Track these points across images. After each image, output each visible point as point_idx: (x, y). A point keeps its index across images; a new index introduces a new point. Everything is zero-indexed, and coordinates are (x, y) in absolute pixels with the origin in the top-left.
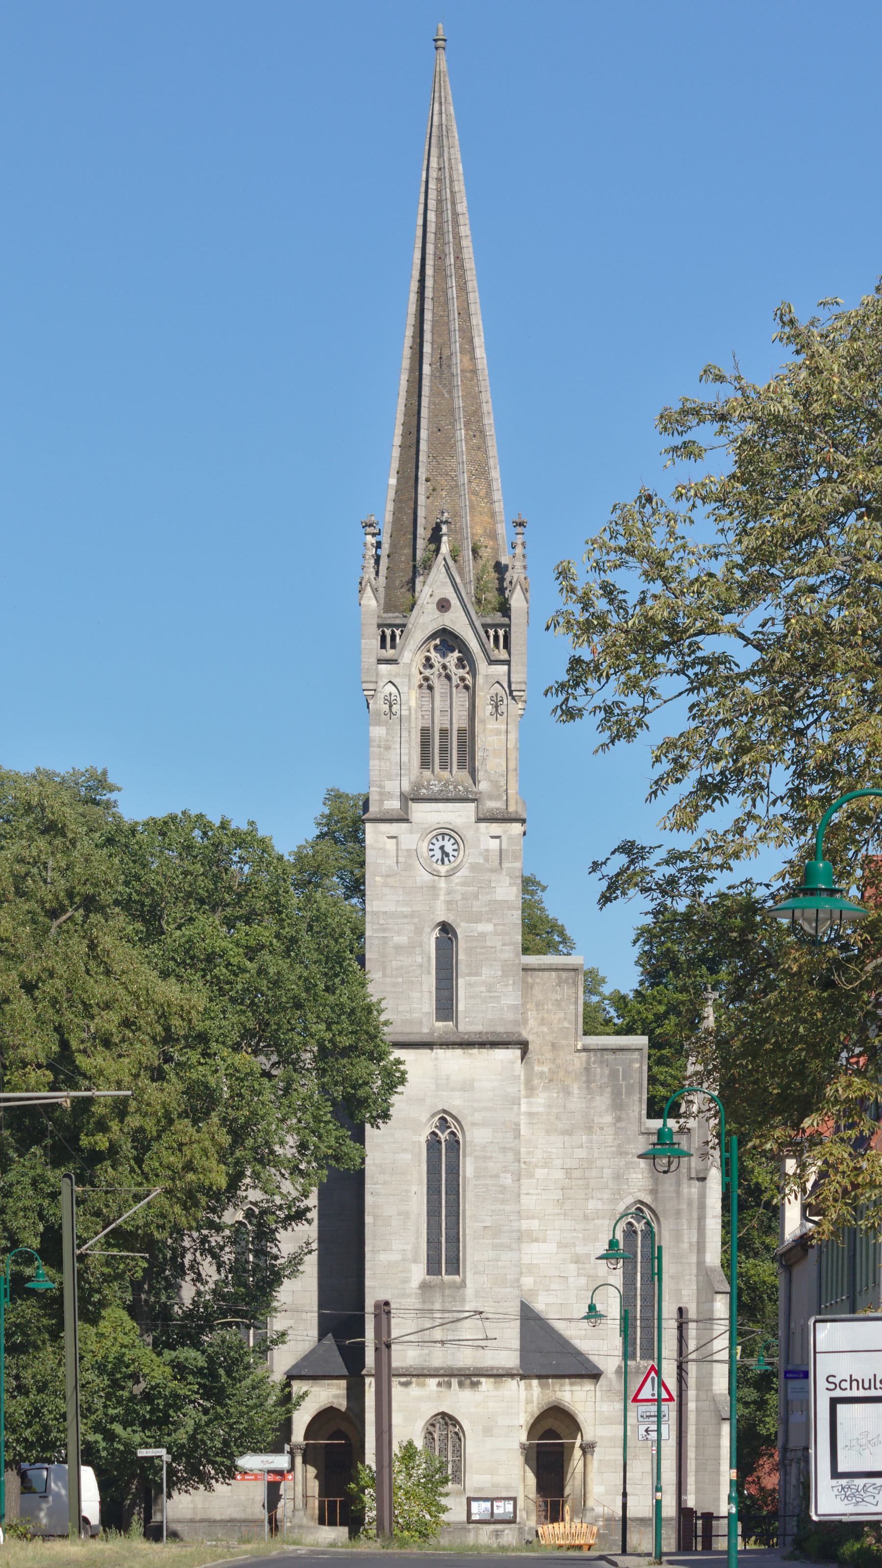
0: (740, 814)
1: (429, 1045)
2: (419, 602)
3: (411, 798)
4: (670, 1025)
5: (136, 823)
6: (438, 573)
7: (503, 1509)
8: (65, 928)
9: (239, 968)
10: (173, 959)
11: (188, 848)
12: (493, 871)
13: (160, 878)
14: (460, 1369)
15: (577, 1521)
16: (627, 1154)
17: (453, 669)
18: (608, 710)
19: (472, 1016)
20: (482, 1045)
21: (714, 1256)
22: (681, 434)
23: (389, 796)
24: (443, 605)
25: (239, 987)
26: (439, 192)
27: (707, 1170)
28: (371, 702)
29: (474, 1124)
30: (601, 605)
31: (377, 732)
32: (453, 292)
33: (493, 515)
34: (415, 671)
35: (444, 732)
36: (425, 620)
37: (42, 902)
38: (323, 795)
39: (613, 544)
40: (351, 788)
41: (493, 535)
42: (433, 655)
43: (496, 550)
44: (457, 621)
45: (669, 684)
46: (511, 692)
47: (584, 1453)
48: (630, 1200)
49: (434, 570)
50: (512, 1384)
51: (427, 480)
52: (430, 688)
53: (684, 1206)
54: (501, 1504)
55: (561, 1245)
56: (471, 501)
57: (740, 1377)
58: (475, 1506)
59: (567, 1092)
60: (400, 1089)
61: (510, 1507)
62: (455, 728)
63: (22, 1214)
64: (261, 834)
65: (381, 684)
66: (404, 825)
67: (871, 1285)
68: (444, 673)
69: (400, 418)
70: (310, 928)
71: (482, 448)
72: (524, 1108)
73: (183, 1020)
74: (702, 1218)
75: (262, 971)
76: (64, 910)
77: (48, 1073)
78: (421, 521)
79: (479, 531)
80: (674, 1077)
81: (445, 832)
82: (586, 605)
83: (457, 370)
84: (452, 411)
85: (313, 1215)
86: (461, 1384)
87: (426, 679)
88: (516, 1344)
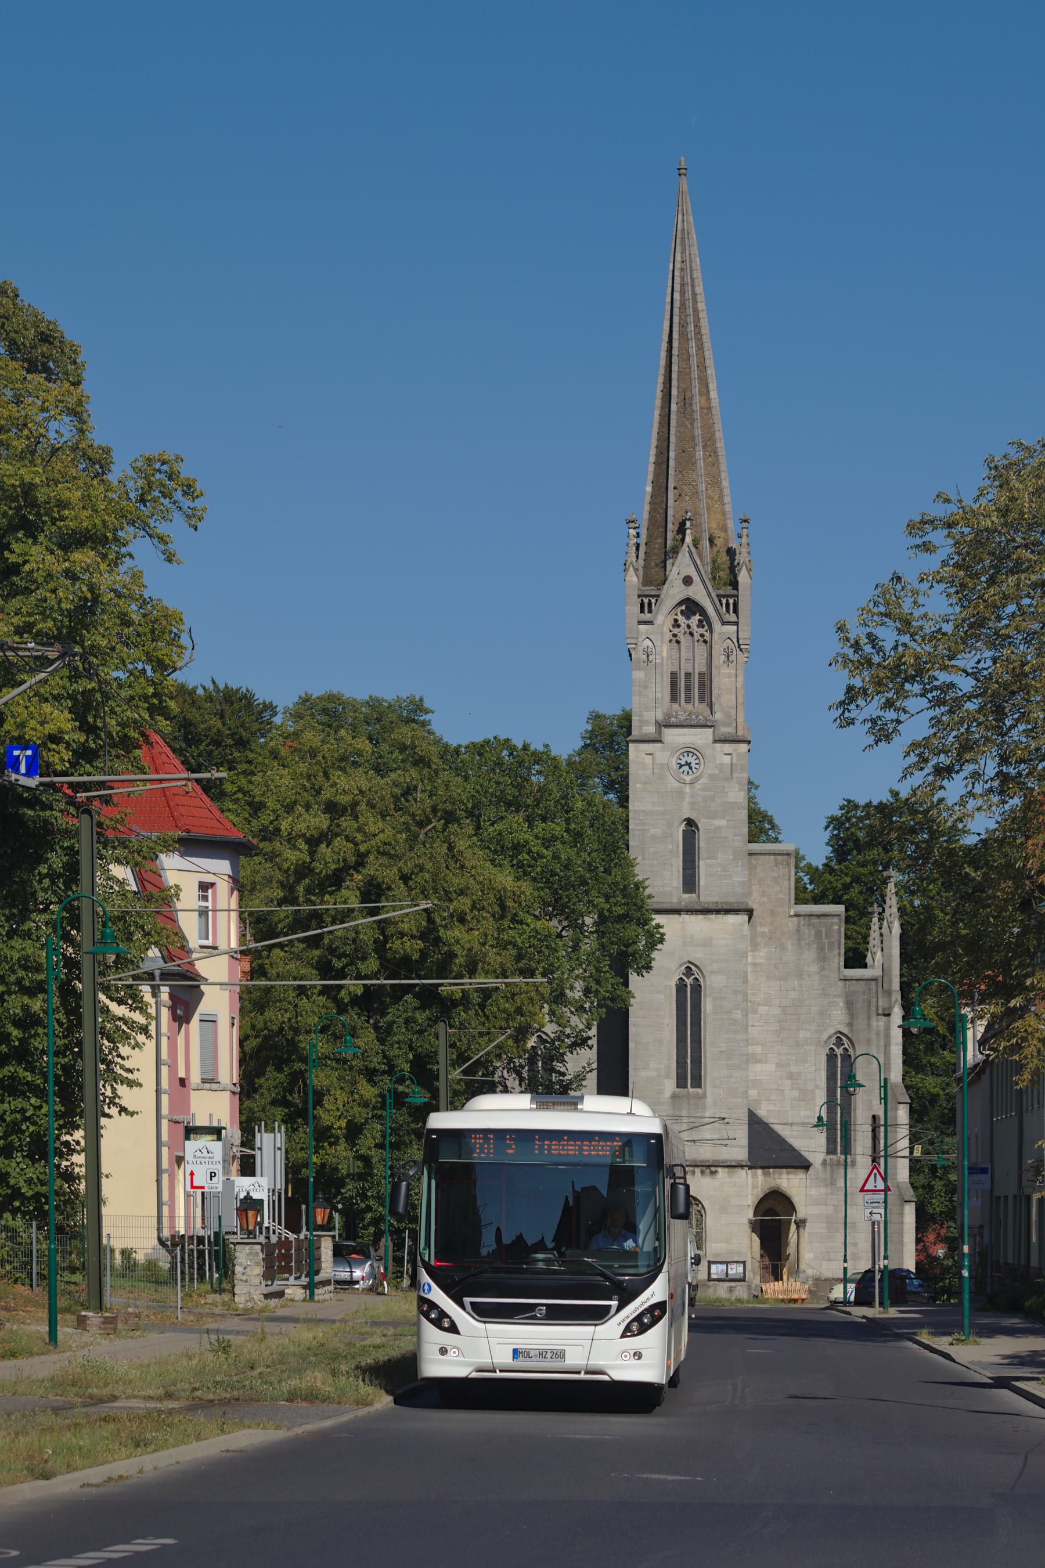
0: (964, 792)
1: (677, 912)
2: (670, 579)
3: (663, 725)
4: (855, 891)
5: (460, 746)
6: (683, 557)
7: (736, 1270)
8: (430, 834)
9: (538, 854)
10: (488, 848)
11: (499, 764)
12: (725, 779)
13: (478, 787)
14: (702, 1161)
15: (792, 1280)
16: (829, 995)
17: (695, 628)
18: (874, 721)
19: (709, 891)
20: (718, 912)
21: (896, 1074)
22: (921, 537)
23: (647, 723)
24: (688, 581)
25: (539, 869)
26: (682, 278)
27: (891, 1008)
28: (633, 653)
29: (712, 972)
30: (868, 649)
31: (638, 675)
32: (693, 351)
33: (724, 513)
34: (666, 630)
35: (688, 675)
36: (674, 592)
37: (413, 815)
38: (587, 715)
39: (876, 610)
40: (612, 710)
41: (724, 529)
42: (680, 618)
43: (726, 540)
44: (698, 593)
45: (915, 704)
46: (739, 646)
47: (798, 1227)
48: (832, 1031)
49: (680, 556)
50: (743, 1174)
51: (675, 488)
52: (678, 642)
53: (873, 1036)
54: (734, 1266)
55: (779, 1065)
56: (707, 504)
57: (915, 1167)
58: (713, 1267)
59: (782, 947)
60: (659, 946)
61: (740, 1269)
62: (697, 672)
63: (397, 1046)
64: (553, 754)
65: (641, 639)
66: (659, 745)
67: (1036, 1106)
68: (688, 631)
69: (654, 442)
70: (592, 826)
71: (715, 464)
72: (750, 960)
73: (515, 902)
74: (887, 1045)
75: (556, 857)
76: (429, 822)
77: (419, 942)
78: (670, 519)
79: (714, 525)
80: (859, 933)
81: (691, 750)
82: (857, 646)
83: (697, 407)
84: (693, 438)
85: (593, 1042)
86: (702, 1172)
87: (675, 635)
88: (745, 1142)
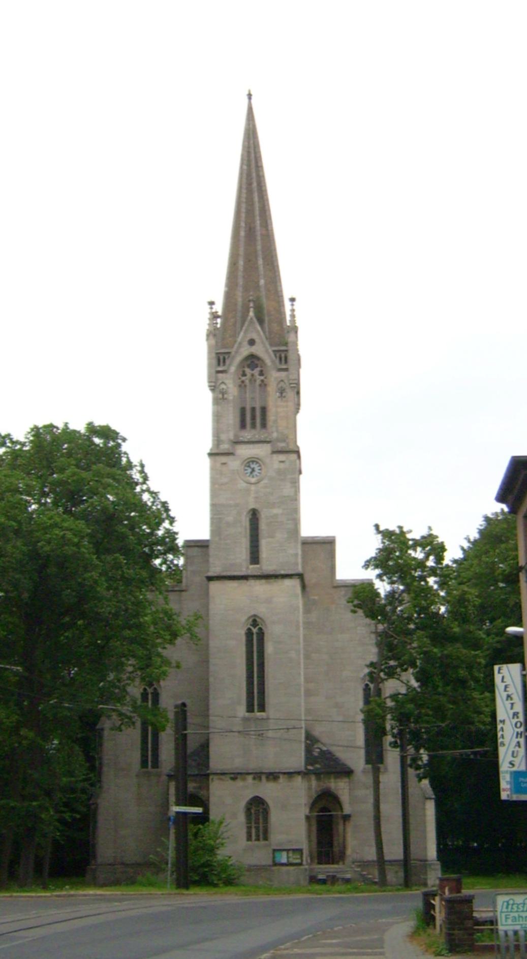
32: (256, 199)
35: (253, 409)
66: (231, 457)
83: (258, 233)
